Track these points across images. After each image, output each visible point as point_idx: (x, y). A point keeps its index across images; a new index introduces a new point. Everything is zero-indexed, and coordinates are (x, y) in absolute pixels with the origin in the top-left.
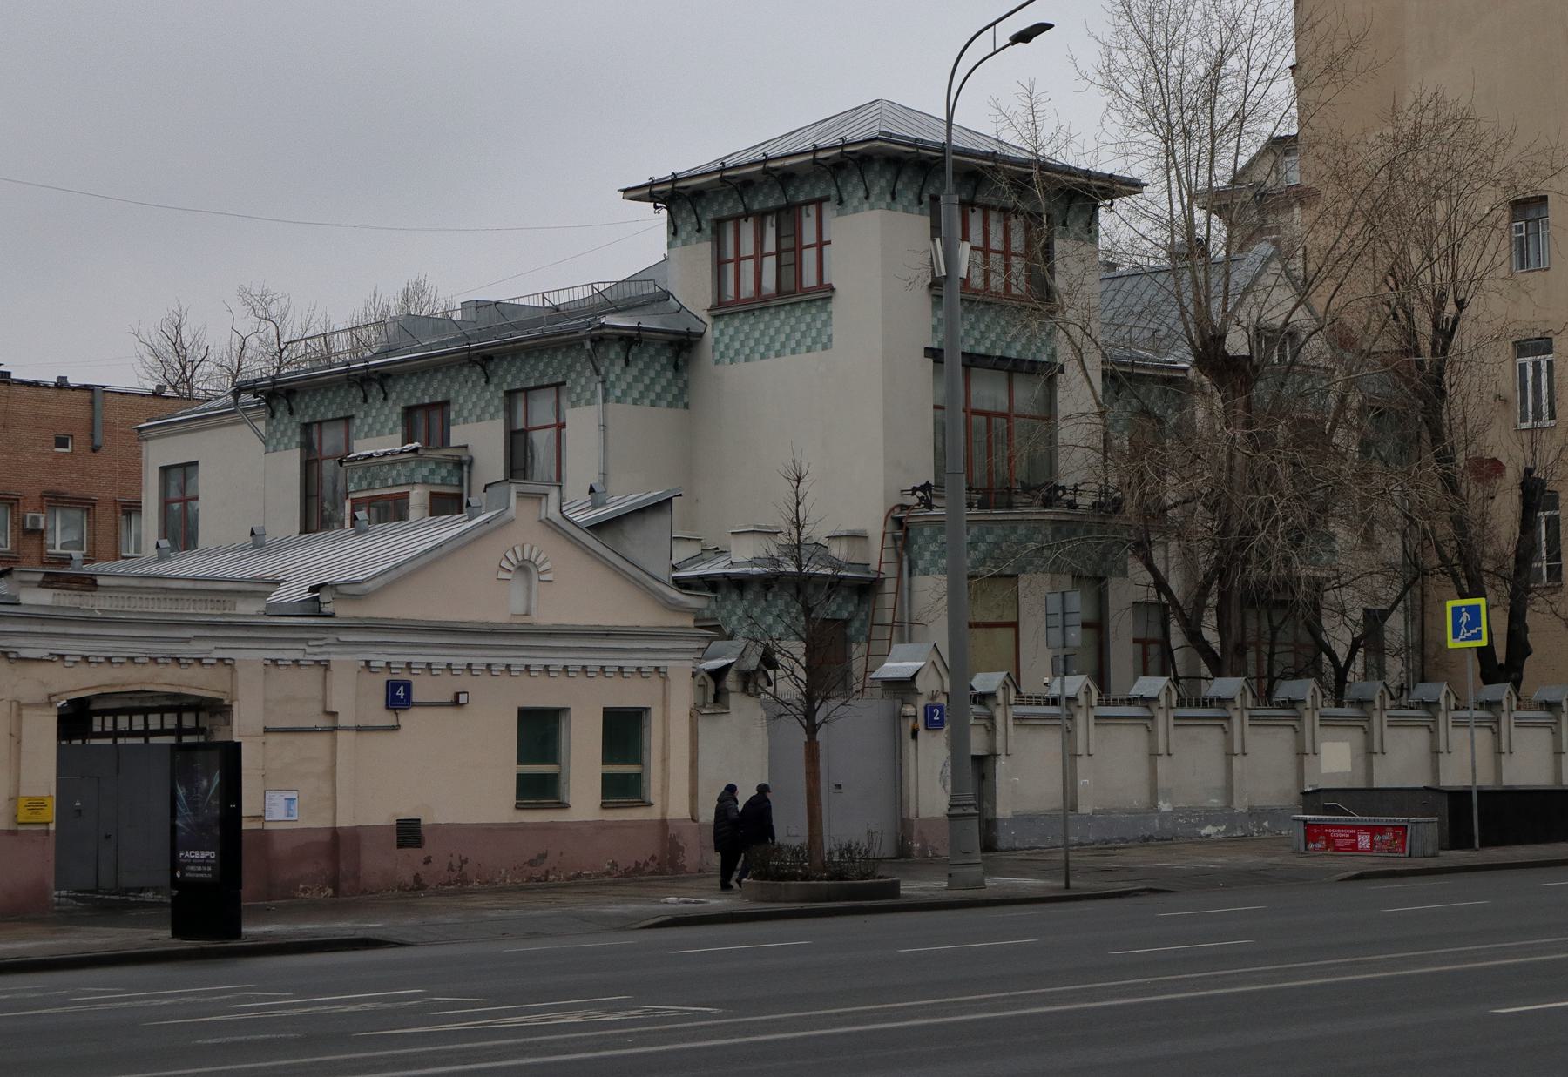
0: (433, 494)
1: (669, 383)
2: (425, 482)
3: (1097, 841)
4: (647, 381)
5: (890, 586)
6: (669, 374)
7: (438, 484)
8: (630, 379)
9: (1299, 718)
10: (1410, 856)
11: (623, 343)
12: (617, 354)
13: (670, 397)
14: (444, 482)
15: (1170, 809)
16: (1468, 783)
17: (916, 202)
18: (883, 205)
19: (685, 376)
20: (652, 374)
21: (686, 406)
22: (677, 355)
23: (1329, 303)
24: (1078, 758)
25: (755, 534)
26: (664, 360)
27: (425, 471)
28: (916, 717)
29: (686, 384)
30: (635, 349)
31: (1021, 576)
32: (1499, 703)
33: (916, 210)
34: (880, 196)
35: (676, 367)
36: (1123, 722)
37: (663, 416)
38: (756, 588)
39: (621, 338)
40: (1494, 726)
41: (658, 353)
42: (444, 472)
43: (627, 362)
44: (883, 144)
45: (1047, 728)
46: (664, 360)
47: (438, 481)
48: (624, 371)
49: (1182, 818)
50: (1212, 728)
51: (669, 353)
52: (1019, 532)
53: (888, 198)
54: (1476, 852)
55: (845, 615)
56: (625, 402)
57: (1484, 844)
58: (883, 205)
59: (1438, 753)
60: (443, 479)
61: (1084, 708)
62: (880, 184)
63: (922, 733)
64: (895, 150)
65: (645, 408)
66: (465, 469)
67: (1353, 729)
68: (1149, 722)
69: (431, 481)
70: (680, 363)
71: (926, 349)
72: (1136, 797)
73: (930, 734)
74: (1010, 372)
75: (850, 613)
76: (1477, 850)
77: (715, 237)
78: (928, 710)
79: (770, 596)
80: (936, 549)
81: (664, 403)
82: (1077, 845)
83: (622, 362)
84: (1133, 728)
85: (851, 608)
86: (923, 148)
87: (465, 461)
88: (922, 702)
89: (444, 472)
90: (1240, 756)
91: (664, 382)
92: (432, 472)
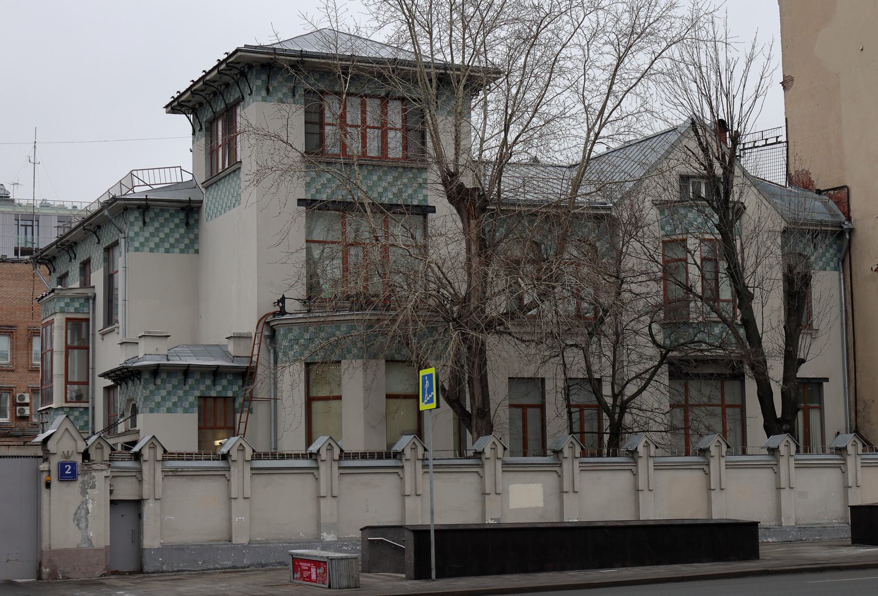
0: (68, 320)
1: (182, 236)
2: (62, 311)
3: (253, 565)
4: (162, 235)
5: (261, 372)
6: (182, 231)
7: (72, 313)
8: (147, 234)
9: (482, 466)
10: (330, 587)
11: (141, 210)
12: (136, 219)
13: (182, 246)
14: (77, 311)
15: (336, 539)
16: (427, 522)
17: (290, 94)
18: (259, 98)
19: (196, 231)
20: (167, 230)
21: (197, 252)
22: (187, 216)
23: (690, 151)
24: (640, 492)
25: (146, 337)
26: (177, 221)
27: (62, 304)
28: (49, 471)
29: (197, 237)
30: (151, 214)
31: (342, 361)
32: (845, 448)
33: (291, 100)
34: (259, 89)
35: (187, 224)
36: (812, 466)
37: (176, 259)
38: (146, 376)
39: (139, 207)
40: (705, 468)
41: (172, 215)
42: (77, 305)
43: (144, 223)
44: (243, 53)
45: (206, 477)
46: (177, 221)
47: (72, 310)
48: (142, 229)
49: (347, 546)
50: (387, 475)
51: (182, 215)
52: (342, 329)
53: (264, 93)
54: (434, 583)
55: (230, 394)
56: (143, 251)
57: (439, 576)
58: (259, 98)
59: (637, 490)
60: (76, 309)
61: (570, 459)
62: (257, 83)
63: (55, 482)
64: (266, 58)
65: (160, 255)
66: (91, 301)
67: (544, 473)
68: (315, 472)
69: (81, 311)
70: (192, 222)
71: (299, 200)
72: (303, 528)
73: (64, 484)
74: (344, 211)
75: (234, 392)
76: (434, 580)
77: (209, 133)
78: (62, 467)
79: (159, 382)
80: (287, 344)
81: (177, 250)
82: (230, 568)
83: (141, 223)
84: (299, 476)
85: (236, 388)
86: (280, 55)
87: (90, 296)
88: (55, 461)
89: (77, 305)
90: (571, 494)
91: (177, 236)
92: (67, 305)
